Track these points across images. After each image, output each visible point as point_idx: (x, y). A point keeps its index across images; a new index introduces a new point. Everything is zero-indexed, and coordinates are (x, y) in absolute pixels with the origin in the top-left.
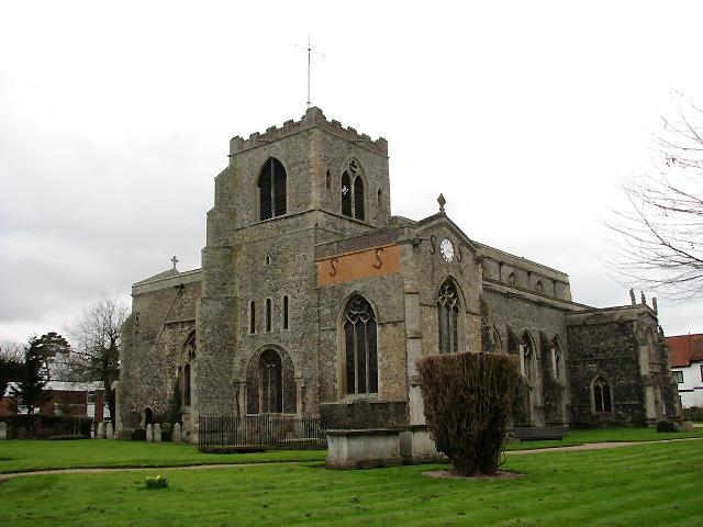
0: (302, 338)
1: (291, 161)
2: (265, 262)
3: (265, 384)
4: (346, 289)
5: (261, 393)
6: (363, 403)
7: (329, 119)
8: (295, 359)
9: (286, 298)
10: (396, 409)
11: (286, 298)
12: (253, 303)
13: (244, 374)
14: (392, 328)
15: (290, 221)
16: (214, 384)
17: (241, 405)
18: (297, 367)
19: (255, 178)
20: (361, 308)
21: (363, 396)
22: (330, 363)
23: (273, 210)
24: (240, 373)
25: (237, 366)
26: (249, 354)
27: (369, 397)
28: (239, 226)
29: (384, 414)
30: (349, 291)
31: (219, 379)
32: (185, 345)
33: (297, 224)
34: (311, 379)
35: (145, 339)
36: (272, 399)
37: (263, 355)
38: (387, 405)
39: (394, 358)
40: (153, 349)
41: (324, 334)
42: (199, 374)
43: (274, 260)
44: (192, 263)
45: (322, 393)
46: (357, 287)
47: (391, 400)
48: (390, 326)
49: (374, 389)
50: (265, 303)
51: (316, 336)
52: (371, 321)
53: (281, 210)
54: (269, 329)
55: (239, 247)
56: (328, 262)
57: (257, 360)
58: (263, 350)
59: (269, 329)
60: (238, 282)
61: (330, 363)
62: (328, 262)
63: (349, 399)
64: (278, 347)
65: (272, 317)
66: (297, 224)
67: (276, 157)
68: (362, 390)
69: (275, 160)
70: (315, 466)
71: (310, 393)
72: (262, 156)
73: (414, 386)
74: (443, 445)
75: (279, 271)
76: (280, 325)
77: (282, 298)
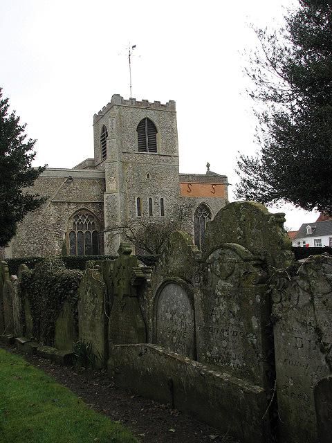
12: (138, 198)
33: (168, 161)
54: (151, 214)
69: (149, 120)
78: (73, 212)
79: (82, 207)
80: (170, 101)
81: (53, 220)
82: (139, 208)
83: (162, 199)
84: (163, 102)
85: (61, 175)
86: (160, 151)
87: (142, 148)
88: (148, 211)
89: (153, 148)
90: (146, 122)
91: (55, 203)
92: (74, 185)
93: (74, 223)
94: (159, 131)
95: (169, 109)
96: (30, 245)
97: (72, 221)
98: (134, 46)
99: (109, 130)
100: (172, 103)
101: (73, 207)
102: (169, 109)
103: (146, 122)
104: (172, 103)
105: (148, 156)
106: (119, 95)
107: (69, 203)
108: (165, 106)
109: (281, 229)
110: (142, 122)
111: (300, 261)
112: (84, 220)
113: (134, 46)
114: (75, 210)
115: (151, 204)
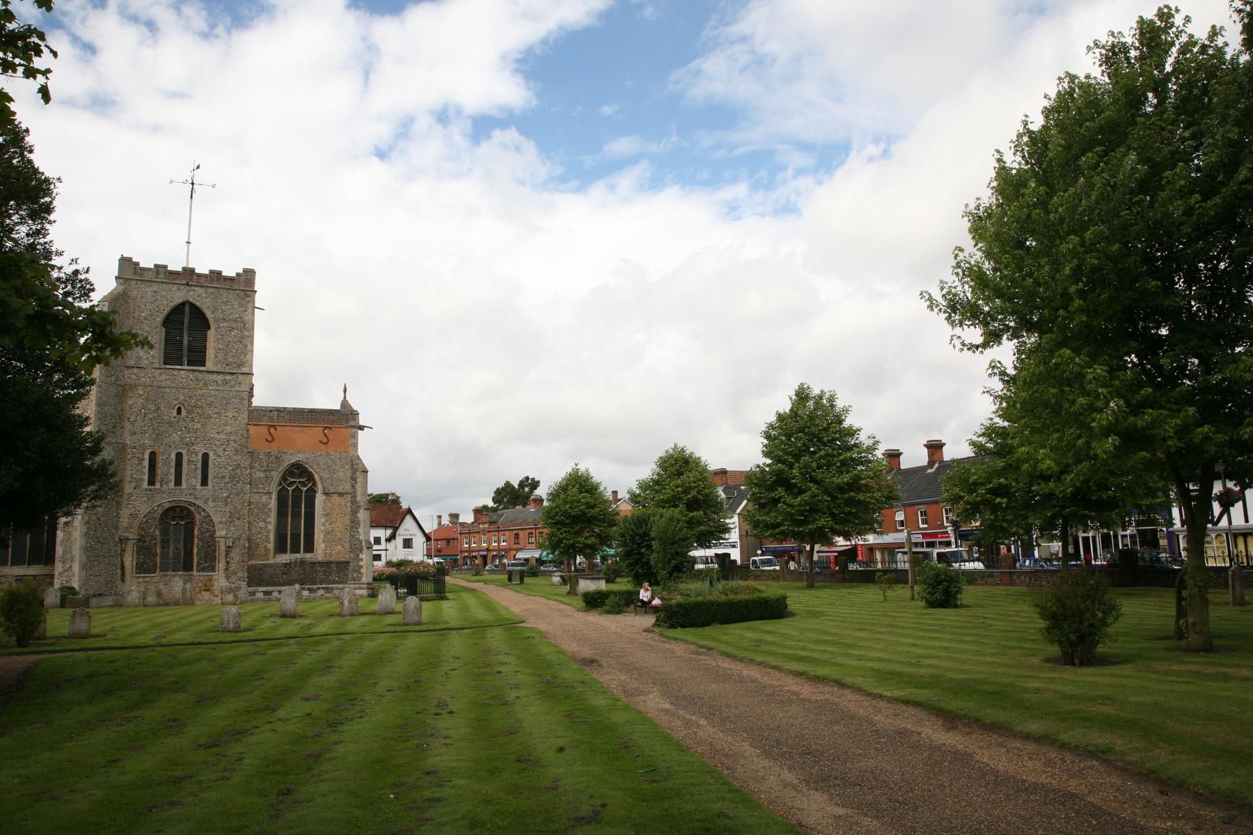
1: (219, 315)
2: (174, 413)
6: (303, 562)
7: (376, 485)
8: (216, 519)
9: (206, 456)
11: (206, 456)
13: (135, 530)
15: (207, 376)
18: (218, 527)
20: (300, 476)
21: (297, 555)
23: (185, 359)
24: (127, 529)
25: (124, 521)
26: (144, 509)
27: (308, 556)
28: (132, 363)
33: (225, 383)
34: (239, 539)
37: (166, 513)
38: (327, 564)
39: (338, 524)
41: (257, 496)
43: (189, 412)
45: (251, 551)
46: (299, 457)
47: (332, 559)
48: (335, 497)
49: (310, 547)
51: (247, 497)
55: (132, 387)
56: (264, 429)
57: (157, 516)
58: (167, 506)
59: (178, 482)
60: (128, 426)
61: (262, 524)
66: (225, 383)
68: (295, 550)
69: (192, 305)
71: (236, 555)
72: (178, 295)
74: (859, 489)
75: (198, 426)
76: (197, 481)
77: (200, 455)
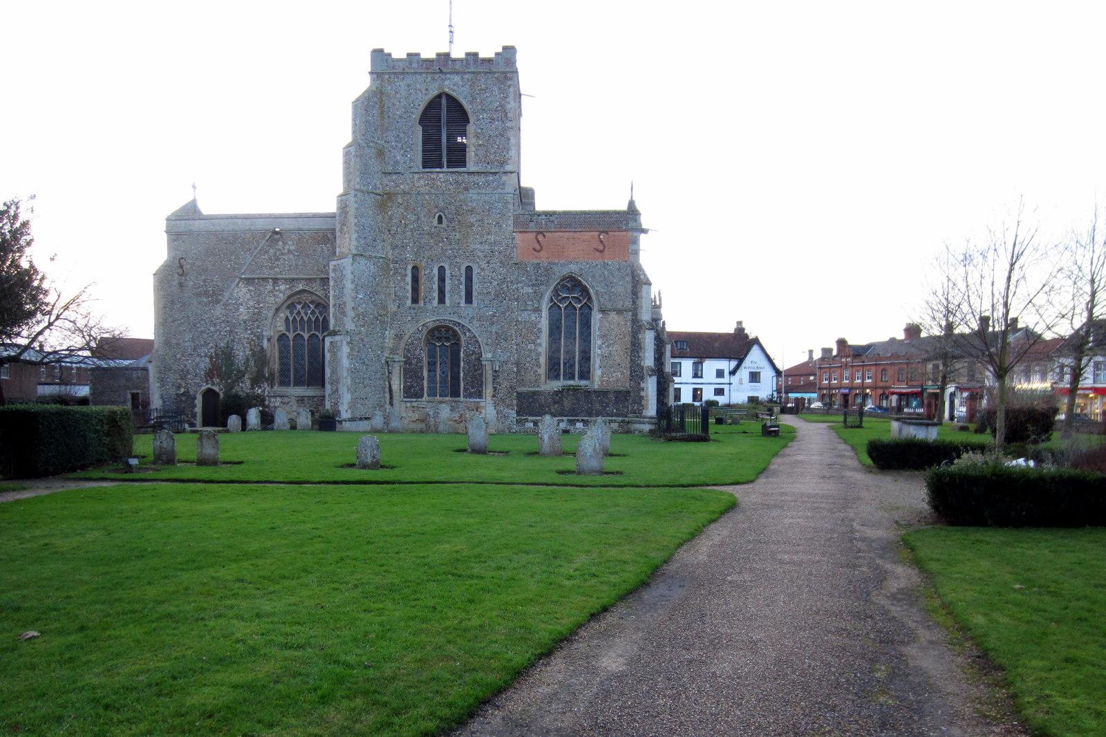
0: (493, 316)
3: (432, 365)
4: (556, 269)
5: (425, 374)
10: (617, 397)
12: (415, 269)
13: (401, 352)
14: (616, 317)
16: (367, 362)
17: (395, 387)
19: (417, 115)
21: (571, 382)
22: (531, 346)
29: (601, 402)
30: (561, 271)
31: (371, 356)
32: (277, 310)
33: (488, 184)
35: (198, 295)
36: (443, 381)
37: (432, 332)
40: (218, 311)
42: (352, 349)
43: (451, 221)
44: (542, 204)
46: (574, 268)
48: (613, 315)
50: (436, 271)
52: (588, 308)
53: (462, 162)
54: (442, 300)
56: (532, 236)
59: (442, 300)
61: (531, 346)
62: (532, 236)
63: (556, 385)
64: (456, 323)
65: (448, 288)
67: (451, 92)
69: (449, 97)
70: (376, 465)
73: (650, 376)
78: (282, 297)
79: (300, 287)
80: (505, 48)
81: (244, 314)
82: (415, 289)
83: (469, 269)
84: (487, 52)
85: (260, 225)
86: (471, 166)
87: (431, 160)
88: (436, 295)
89: (458, 157)
90: (444, 101)
91: (249, 281)
92: (285, 244)
93: (287, 318)
94: (472, 119)
95: (499, 72)
96: (198, 359)
97: (282, 315)
98: (52, 259)
99: (241, 465)
100: (508, 53)
101: (282, 287)
102: (499, 72)
103: (444, 101)
104: (508, 53)
105: (443, 176)
106: (381, 51)
107: (275, 280)
108: (489, 61)
109: (982, 612)
110: (434, 104)
111: (790, 395)
112: (306, 314)
113: (52, 259)
114: (289, 293)
115: (442, 279)
